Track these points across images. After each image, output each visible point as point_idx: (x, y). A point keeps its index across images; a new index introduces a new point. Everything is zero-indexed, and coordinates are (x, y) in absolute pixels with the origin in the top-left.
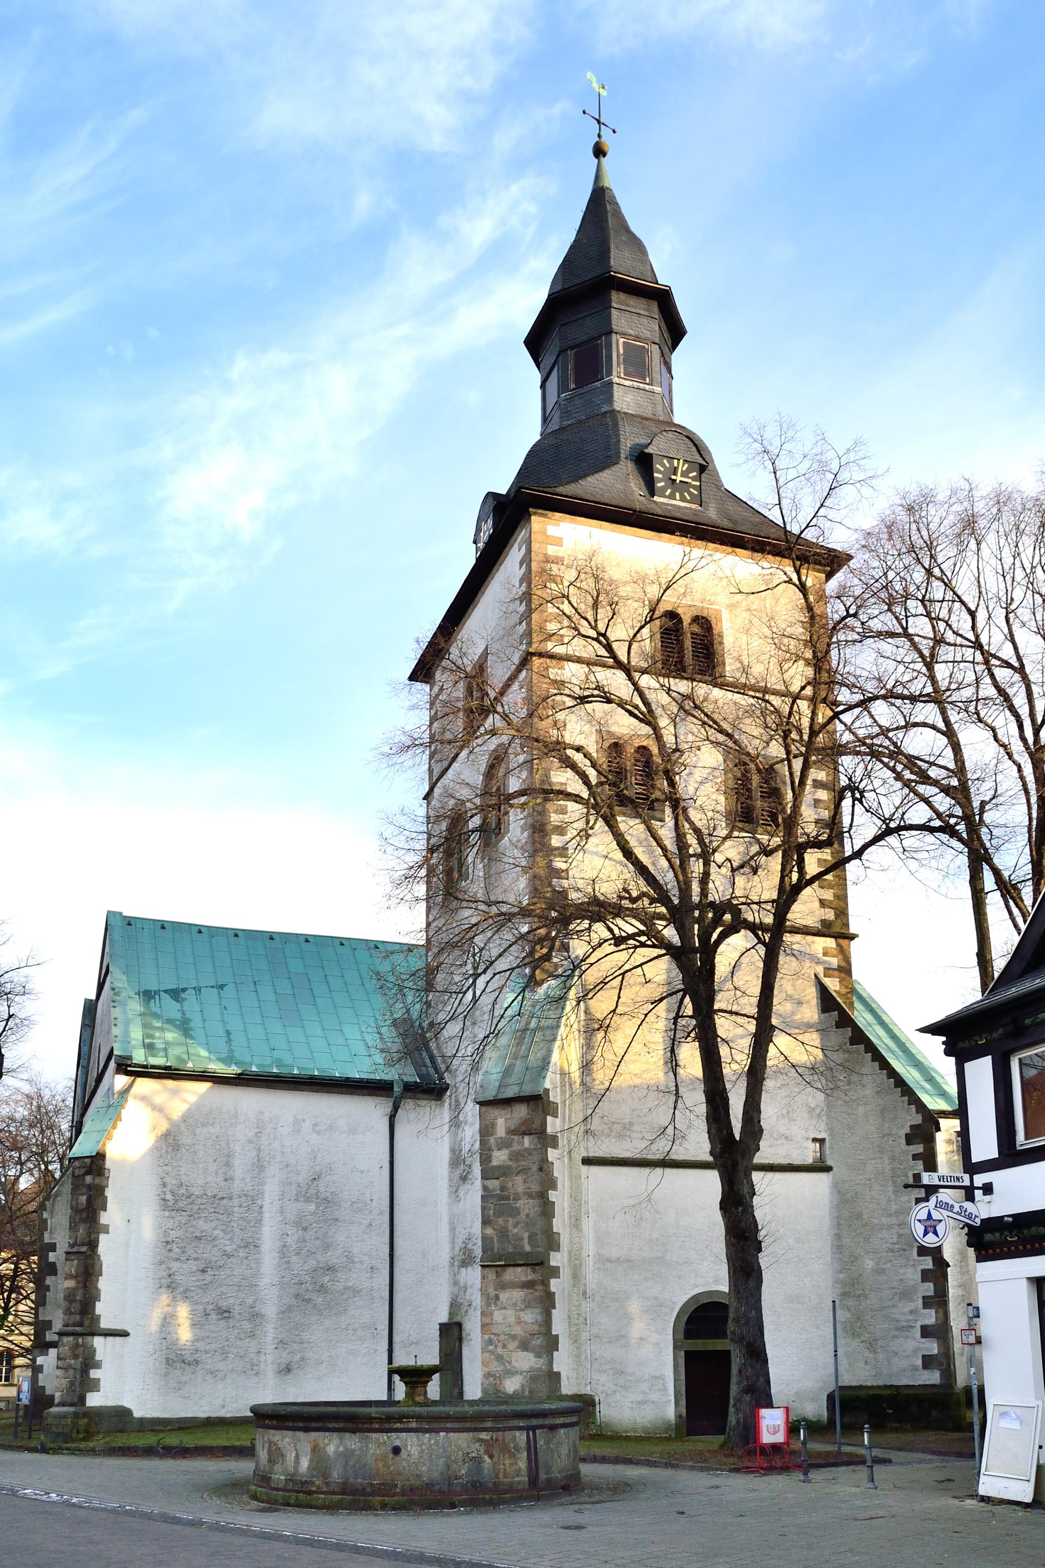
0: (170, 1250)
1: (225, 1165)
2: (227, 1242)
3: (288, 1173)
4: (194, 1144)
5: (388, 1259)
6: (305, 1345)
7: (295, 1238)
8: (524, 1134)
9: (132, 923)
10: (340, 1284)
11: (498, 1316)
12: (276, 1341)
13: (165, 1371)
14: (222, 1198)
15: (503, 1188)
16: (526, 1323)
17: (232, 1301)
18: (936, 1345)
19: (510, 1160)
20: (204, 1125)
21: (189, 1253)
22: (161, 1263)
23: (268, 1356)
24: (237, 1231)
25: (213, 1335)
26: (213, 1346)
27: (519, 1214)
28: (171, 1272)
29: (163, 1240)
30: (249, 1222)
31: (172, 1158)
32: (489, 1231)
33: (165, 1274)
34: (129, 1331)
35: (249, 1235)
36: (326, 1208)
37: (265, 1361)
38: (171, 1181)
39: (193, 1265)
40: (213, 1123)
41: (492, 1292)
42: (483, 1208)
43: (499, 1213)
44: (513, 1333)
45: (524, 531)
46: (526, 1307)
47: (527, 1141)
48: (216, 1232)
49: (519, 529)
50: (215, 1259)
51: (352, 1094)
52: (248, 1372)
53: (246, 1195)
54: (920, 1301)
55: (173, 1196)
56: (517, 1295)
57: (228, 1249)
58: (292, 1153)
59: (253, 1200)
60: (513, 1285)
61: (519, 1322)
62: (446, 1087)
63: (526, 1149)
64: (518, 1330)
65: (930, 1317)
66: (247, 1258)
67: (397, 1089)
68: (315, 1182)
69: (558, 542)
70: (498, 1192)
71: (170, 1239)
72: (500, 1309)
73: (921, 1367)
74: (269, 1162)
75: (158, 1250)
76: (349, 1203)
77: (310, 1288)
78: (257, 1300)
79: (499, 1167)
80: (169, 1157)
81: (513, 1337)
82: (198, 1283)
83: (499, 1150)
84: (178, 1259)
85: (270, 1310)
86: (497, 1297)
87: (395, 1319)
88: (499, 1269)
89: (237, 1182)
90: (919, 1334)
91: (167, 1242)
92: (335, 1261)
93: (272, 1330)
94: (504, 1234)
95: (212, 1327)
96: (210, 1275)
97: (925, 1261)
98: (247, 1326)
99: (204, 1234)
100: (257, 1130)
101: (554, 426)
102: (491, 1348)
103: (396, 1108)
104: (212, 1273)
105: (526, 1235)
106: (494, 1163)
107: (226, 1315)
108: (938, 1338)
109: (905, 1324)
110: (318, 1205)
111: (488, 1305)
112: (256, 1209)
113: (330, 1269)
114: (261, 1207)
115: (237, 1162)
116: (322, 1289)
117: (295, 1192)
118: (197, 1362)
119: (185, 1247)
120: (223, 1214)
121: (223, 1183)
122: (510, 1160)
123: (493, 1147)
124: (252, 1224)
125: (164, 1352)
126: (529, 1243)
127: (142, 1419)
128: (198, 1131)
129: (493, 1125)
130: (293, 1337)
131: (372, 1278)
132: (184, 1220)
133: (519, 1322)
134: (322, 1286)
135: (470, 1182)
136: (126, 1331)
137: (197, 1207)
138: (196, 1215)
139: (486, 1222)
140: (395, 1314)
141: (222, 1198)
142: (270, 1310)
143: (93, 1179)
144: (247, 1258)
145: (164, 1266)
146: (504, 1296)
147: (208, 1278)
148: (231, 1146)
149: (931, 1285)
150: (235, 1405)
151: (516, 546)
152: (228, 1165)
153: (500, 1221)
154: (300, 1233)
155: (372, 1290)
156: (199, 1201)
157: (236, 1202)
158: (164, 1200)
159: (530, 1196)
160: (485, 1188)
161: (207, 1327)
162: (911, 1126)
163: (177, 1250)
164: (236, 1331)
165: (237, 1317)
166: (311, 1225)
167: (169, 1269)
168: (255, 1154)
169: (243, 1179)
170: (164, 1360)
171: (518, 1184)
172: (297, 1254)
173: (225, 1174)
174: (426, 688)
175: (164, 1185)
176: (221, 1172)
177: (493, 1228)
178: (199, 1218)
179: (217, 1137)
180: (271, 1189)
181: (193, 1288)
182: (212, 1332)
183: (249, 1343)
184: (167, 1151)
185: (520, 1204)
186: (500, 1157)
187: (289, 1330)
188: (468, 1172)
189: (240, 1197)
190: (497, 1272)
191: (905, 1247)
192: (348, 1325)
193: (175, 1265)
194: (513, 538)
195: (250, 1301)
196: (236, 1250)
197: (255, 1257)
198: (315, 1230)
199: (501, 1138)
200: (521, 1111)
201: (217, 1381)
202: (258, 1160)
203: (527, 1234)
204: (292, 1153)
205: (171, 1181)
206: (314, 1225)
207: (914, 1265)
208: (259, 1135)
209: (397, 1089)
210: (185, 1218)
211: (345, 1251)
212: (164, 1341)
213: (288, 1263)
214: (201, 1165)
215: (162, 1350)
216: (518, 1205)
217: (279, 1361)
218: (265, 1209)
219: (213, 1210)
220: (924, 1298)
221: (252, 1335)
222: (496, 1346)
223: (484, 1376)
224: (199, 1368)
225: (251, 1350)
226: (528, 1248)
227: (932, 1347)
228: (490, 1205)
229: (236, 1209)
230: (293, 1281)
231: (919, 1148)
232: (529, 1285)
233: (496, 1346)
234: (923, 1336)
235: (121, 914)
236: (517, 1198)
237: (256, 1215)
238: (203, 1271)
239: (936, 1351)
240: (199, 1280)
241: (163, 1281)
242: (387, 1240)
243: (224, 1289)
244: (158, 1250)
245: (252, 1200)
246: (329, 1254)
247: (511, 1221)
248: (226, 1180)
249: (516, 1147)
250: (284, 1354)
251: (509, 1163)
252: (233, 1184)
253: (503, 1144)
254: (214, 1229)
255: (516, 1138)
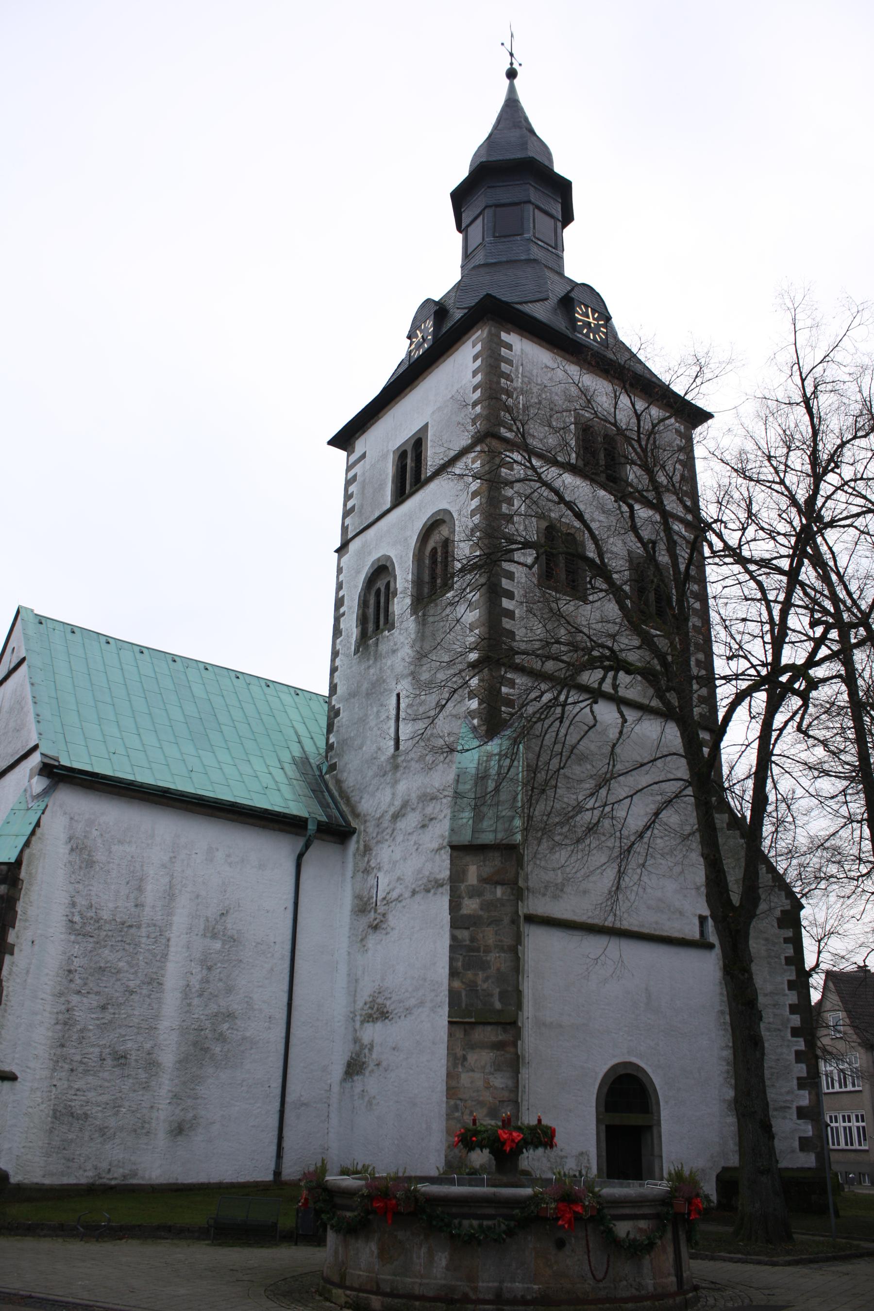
0: (71, 981)
1: (137, 889)
2: (132, 977)
3: (198, 905)
4: (109, 863)
5: (286, 1009)
6: (199, 1101)
7: (199, 977)
8: (498, 883)
9: (43, 622)
10: (239, 1033)
11: (465, 1079)
12: (170, 1094)
13: (51, 1125)
14: (131, 926)
15: (473, 939)
16: (496, 1088)
17: (129, 1045)
18: (810, 1127)
19: (481, 909)
20: (121, 842)
21: (91, 985)
22: (61, 994)
23: (160, 1111)
24: (142, 963)
25: (106, 1084)
26: (105, 1098)
27: (490, 968)
28: (70, 1006)
29: (66, 968)
30: (155, 956)
31: (85, 875)
32: (457, 984)
33: (63, 1007)
34: (18, 1074)
35: (154, 970)
36: (230, 947)
37: (158, 1118)
38: (81, 901)
39: (94, 1001)
40: (130, 842)
41: (460, 1052)
42: (452, 960)
43: (468, 966)
44: (481, 1098)
45: (479, 332)
46: (495, 1070)
47: (499, 891)
48: (121, 964)
49: (475, 329)
50: (117, 994)
51: (264, 827)
52: (139, 1131)
53: (155, 925)
54: (795, 1082)
55: (82, 918)
56: (485, 1057)
57: (132, 984)
58: (204, 883)
59: (161, 931)
60: (482, 1046)
61: (488, 1086)
62: (353, 831)
63: (498, 900)
64: (487, 1097)
65: (804, 1099)
66: (149, 996)
67: (312, 827)
68: (223, 918)
69: (509, 347)
70: (468, 943)
71: (72, 968)
72: (467, 1071)
73: (798, 1150)
74: (181, 891)
75: (59, 979)
76: (254, 944)
77: (210, 1036)
78: (155, 1045)
79: (469, 916)
80: (82, 873)
81: (481, 1104)
82: (98, 1022)
83: (470, 898)
84: (79, 992)
85: (168, 1058)
86: (465, 1058)
87: (289, 1076)
88: (467, 1027)
89: (147, 909)
90: (795, 1116)
91: (70, 971)
92: (236, 1006)
93: (167, 1082)
94: (472, 988)
95: (106, 1075)
96: (110, 1014)
97: (797, 1042)
98: (143, 1075)
99: (109, 965)
100: (172, 855)
101: (480, 258)
102: (457, 1114)
103: (307, 846)
104: (112, 1011)
105: (496, 991)
106: (465, 911)
107: (122, 1061)
108: (812, 1120)
109: (783, 1104)
110: (224, 944)
111: (455, 1065)
112: (164, 941)
113: (230, 1016)
114: (168, 940)
115: (149, 887)
116: (221, 1038)
117: (202, 927)
118: (86, 1116)
119: (87, 978)
120: (129, 944)
121: (133, 909)
122: (481, 909)
123: (464, 895)
124: (158, 958)
125: (52, 1102)
126: (500, 1000)
127: (18, 1184)
128: (114, 848)
129: (464, 872)
130: (188, 1090)
131: (269, 1028)
132: (90, 946)
133: (488, 1086)
134: (221, 1034)
135: (384, 932)
136: (14, 1074)
137: (105, 933)
138: (103, 943)
139: (453, 973)
140: (289, 1071)
141: (131, 926)
142: (168, 1058)
143: (9, 890)
144: (149, 996)
145: (62, 999)
146: (472, 1058)
147: (108, 1016)
148: (145, 868)
149: (804, 1066)
150: (121, 1170)
151: (469, 343)
152: (140, 889)
153: (470, 974)
154: (205, 972)
155: (268, 1042)
156: (107, 927)
157: (144, 931)
158: (71, 921)
159: (502, 949)
160: (453, 938)
161: (101, 1074)
162: (782, 911)
163: (79, 981)
164: (131, 1081)
165: (133, 1064)
166: (216, 964)
167: (69, 1002)
168: (167, 880)
169: (153, 907)
170: (51, 1112)
171: (489, 935)
172: (200, 995)
173: (137, 899)
174: (344, 454)
175: (73, 904)
176: (132, 896)
177: (463, 982)
178: (105, 946)
179: (132, 857)
180: (180, 920)
181: (91, 1027)
182: (106, 1080)
183: (143, 1095)
184: (81, 868)
185: (492, 957)
186: (470, 906)
187: (184, 1083)
188: (382, 921)
189: (148, 926)
190: (465, 1031)
191: (780, 1027)
192: (243, 1081)
193: (75, 999)
194: (467, 336)
195: (148, 1046)
196: (139, 986)
197: (158, 995)
198: (218, 971)
199: (473, 886)
200: (495, 862)
201: (105, 1140)
202: (170, 888)
203: (498, 990)
204: (204, 883)
205: (81, 901)
206: (219, 965)
207: (788, 1046)
208: (174, 860)
209: (312, 827)
210: (91, 945)
211: (246, 997)
212: (54, 1089)
213: (189, 1005)
214: (113, 887)
215: (50, 1100)
216: (488, 958)
217: (171, 1119)
218: (172, 943)
219: (120, 939)
220: (799, 1079)
221: (146, 1087)
222: (462, 1113)
223: (449, 1147)
224: (88, 1123)
225: (144, 1104)
226: (498, 1005)
227: (808, 1130)
228: (458, 956)
229: (144, 940)
230: (193, 1026)
231: (789, 933)
232: (498, 1046)
233: (462, 1113)
234: (800, 1117)
235: (32, 611)
236: (487, 951)
237: (163, 947)
238: (104, 1008)
239: (810, 1134)
240: (98, 1019)
241: (60, 1017)
242: (286, 987)
243: (123, 1031)
244: (59, 979)
245: (161, 933)
246: (230, 998)
247: (481, 975)
248: (136, 906)
249: (488, 896)
250: (177, 1111)
251: (481, 913)
252: (143, 911)
253: (474, 893)
254: (119, 960)
255: (488, 886)
